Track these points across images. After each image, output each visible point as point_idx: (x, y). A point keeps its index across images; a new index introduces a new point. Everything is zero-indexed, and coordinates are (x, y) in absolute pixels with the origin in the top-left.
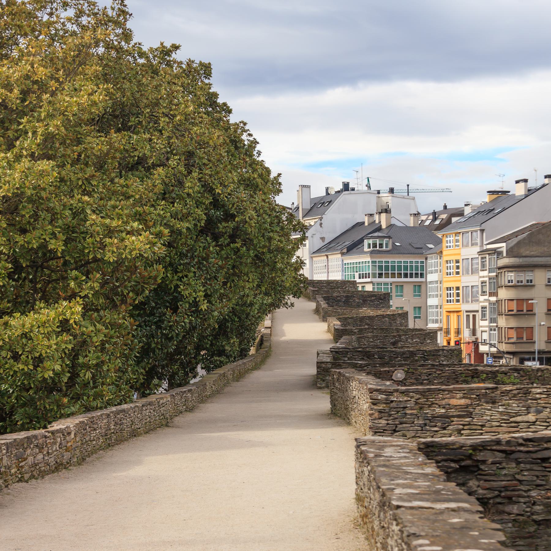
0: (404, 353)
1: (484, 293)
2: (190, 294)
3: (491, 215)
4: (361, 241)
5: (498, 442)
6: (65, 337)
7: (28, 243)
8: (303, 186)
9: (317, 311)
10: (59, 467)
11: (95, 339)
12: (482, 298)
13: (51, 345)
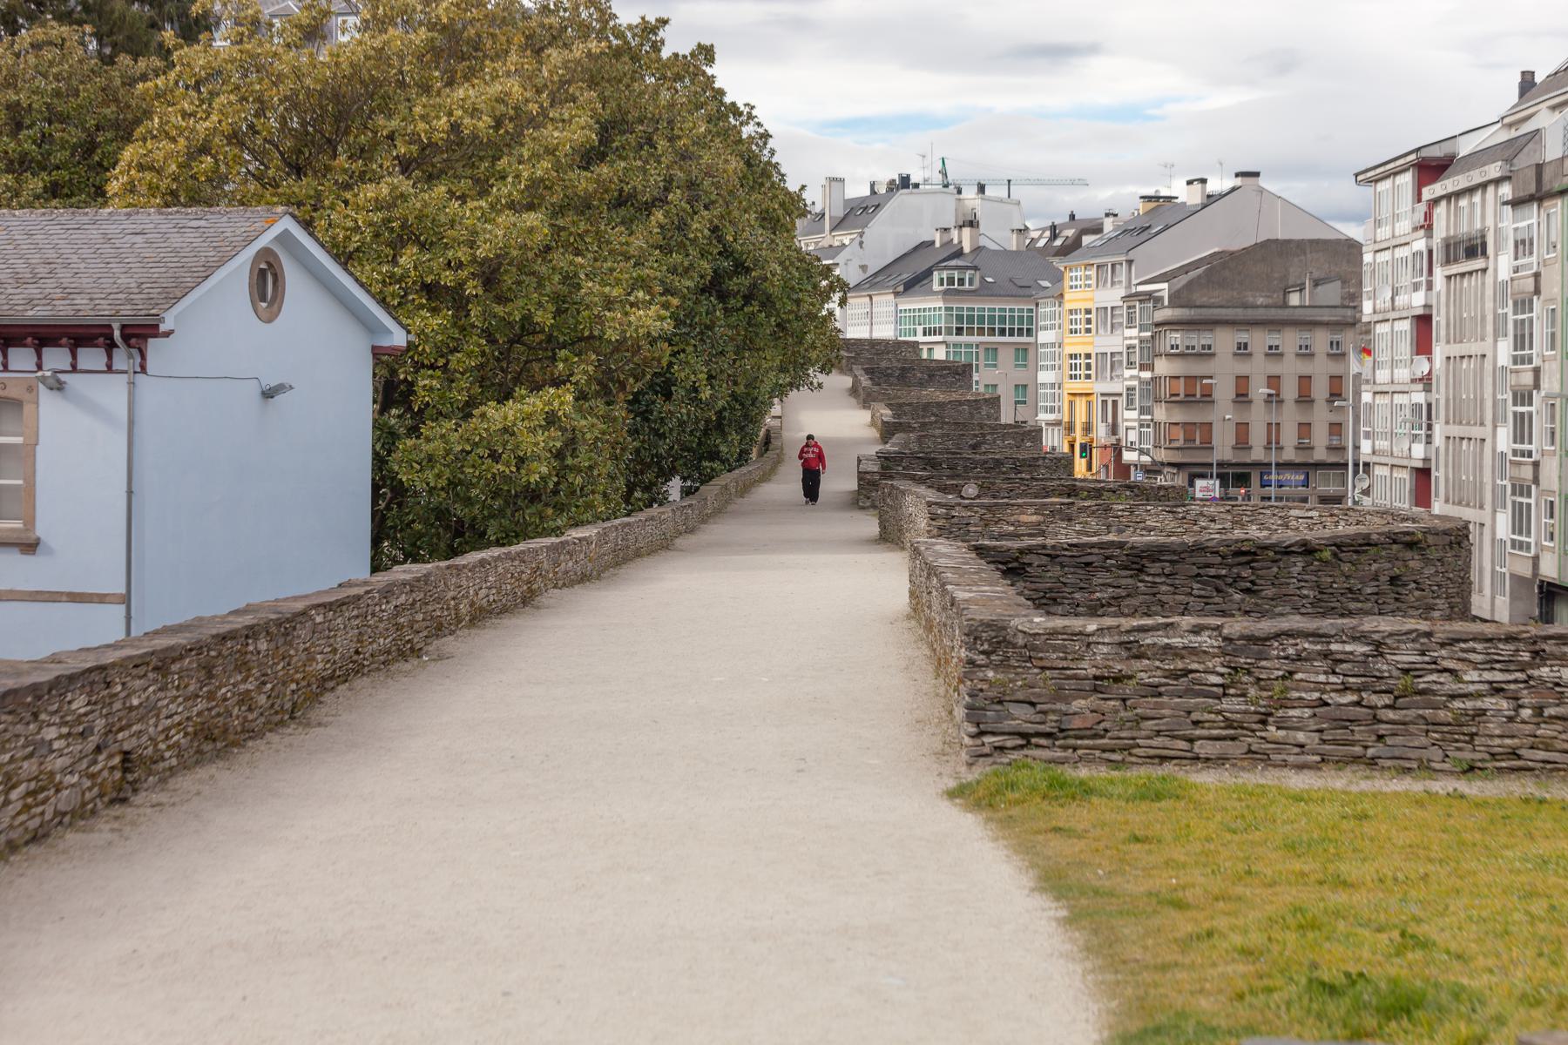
0: (986, 462)
1: (1131, 364)
2: (687, 378)
3: (1145, 235)
4: (928, 274)
5: (1044, 547)
6: (554, 432)
7: (510, 314)
8: (833, 180)
9: (854, 391)
10: (584, 579)
11: (588, 436)
12: (1128, 373)
13: (538, 442)
